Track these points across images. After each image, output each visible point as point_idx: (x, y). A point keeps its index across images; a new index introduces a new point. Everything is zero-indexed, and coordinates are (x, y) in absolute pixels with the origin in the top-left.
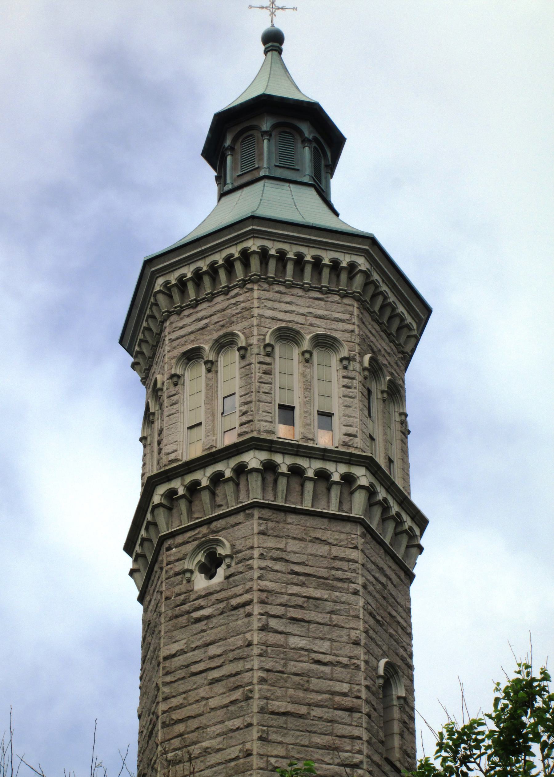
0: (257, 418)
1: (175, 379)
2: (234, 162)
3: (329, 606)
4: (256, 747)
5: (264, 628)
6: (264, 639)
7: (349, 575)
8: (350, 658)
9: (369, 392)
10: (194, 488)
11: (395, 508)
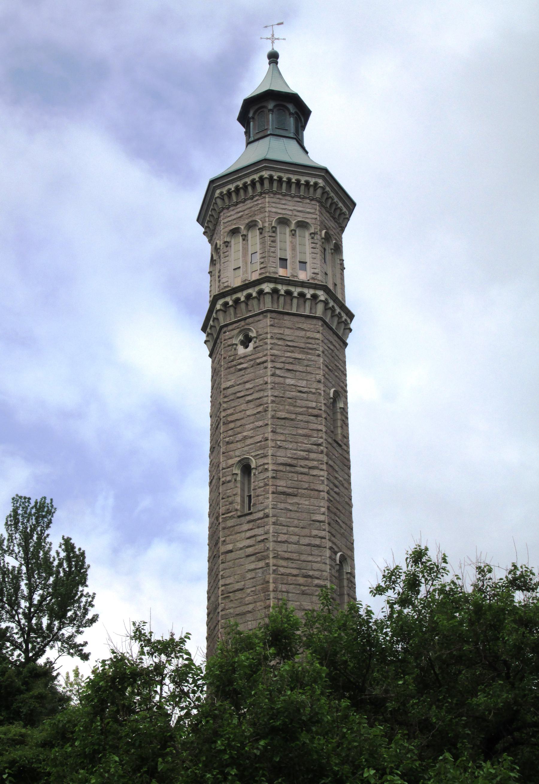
0: (269, 265)
1: (227, 244)
2: (254, 125)
3: (306, 363)
4: (270, 436)
5: (273, 375)
6: (274, 380)
7: (315, 346)
8: (317, 389)
9: (325, 249)
10: (237, 301)
11: (338, 310)
